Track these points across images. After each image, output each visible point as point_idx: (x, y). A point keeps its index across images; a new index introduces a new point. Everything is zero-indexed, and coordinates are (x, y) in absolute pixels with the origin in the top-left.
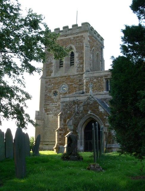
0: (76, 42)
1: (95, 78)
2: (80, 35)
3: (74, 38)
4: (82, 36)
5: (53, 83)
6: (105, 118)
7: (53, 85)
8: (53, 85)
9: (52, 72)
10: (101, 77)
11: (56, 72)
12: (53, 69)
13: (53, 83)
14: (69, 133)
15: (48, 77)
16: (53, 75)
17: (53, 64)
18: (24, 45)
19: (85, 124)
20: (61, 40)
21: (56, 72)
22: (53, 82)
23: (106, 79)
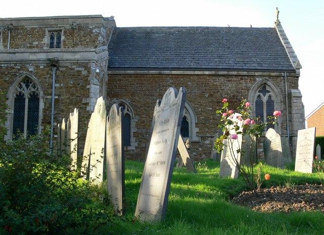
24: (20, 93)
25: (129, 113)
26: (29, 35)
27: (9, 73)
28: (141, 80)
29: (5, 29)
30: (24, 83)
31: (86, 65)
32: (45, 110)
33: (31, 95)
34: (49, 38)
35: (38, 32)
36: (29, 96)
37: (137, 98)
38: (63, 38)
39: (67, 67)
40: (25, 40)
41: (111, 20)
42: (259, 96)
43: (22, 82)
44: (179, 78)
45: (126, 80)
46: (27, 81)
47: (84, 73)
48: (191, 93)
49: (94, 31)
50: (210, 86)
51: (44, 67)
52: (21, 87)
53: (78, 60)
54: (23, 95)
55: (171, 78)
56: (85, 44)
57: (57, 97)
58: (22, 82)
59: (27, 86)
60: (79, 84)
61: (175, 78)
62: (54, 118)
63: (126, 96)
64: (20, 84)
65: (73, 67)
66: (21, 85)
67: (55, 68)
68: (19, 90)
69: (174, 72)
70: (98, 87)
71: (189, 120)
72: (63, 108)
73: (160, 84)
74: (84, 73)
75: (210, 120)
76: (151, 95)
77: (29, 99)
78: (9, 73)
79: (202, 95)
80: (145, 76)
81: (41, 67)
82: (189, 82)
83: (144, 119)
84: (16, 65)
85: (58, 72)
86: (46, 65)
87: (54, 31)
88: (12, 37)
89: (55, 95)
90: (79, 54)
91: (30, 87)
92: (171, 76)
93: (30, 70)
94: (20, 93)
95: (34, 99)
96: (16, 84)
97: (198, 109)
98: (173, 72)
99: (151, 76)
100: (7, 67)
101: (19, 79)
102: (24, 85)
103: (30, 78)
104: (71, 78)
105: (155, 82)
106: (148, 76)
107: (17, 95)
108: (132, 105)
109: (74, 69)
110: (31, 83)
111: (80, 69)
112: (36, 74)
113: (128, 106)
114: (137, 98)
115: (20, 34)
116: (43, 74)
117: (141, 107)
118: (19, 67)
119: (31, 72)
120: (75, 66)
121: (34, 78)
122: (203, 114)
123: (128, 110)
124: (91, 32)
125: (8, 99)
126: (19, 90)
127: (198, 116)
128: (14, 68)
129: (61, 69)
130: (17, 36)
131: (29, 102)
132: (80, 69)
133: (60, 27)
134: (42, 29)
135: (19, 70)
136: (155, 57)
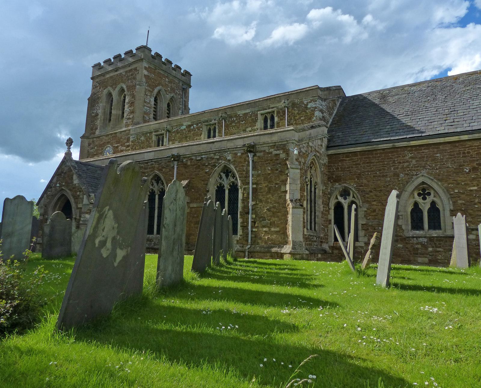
0: (128, 80)
1: (143, 134)
2: (133, 67)
3: (126, 72)
4: (136, 69)
5: (96, 146)
6: (79, 196)
7: (96, 148)
8: (96, 148)
9: (97, 129)
10: (151, 133)
11: (104, 126)
12: (98, 123)
13: (96, 146)
14: (212, 257)
15: (92, 136)
16: (97, 132)
17: (99, 117)
18: (213, 37)
19: (60, 203)
20: (111, 77)
21: (104, 126)
22: (97, 143)
23: (157, 135)
24: (221, 184)
25: (355, 200)
26: (242, 121)
27: (209, 164)
28: (370, 158)
29: (220, 119)
30: (224, 173)
31: (283, 147)
32: (243, 200)
33: (230, 186)
34: (263, 121)
35: (251, 117)
36: (229, 186)
37: (365, 181)
38: (276, 119)
39: (264, 151)
40: (238, 128)
41: (337, 91)
42: (416, 204)
43: (221, 172)
44: (421, 150)
45: (349, 160)
46: (227, 172)
47: (283, 156)
48: (440, 168)
49: (309, 106)
50: (472, 155)
51: (242, 154)
52: (221, 178)
53: (275, 142)
54: (224, 186)
55: (409, 151)
56: (300, 122)
57: (255, 186)
58: (221, 172)
59: (227, 176)
60: (277, 170)
61: (415, 150)
62: (252, 210)
63: (351, 179)
64: (220, 174)
65: (271, 150)
66: (221, 176)
67: (252, 154)
68: (151, 187)
69: (413, 143)
70: (299, 171)
71: (439, 206)
72: (261, 197)
73: (395, 161)
74: (283, 156)
75: (475, 204)
76: (383, 176)
77: (229, 190)
78: (209, 164)
79: (459, 170)
80: (374, 152)
81: (239, 154)
82: (437, 154)
83: (375, 207)
84: (215, 154)
85: (255, 158)
86: (242, 151)
87: (267, 113)
88: (227, 126)
89: (253, 184)
90: (276, 135)
91: (229, 177)
92: (409, 149)
93: (228, 158)
94: (221, 184)
95: (234, 189)
96: (216, 175)
97: (453, 190)
98: (411, 142)
99: (382, 151)
100: (207, 158)
101: (218, 169)
102: (224, 176)
103: (229, 168)
104: (269, 163)
105: (388, 159)
106: (378, 152)
107: (218, 187)
108: (359, 190)
109: (271, 153)
110: (230, 172)
111: (278, 152)
112: (234, 163)
113: (353, 192)
114: (365, 181)
115: (234, 121)
116: (240, 162)
117: (371, 192)
118: (218, 157)
119: (229, 160)
120: (273, 150)
121: (232, 167)
122: (463, 196)
123: (354, 197)
124: (306, 108)
125: (208, 191)
126: (151, 187)
127: (454, 200)
128: (213, 159)
129: (258, 154)
130: (231, 124)
131: (229, 193)
132: (278, 152)
133: (273, 108)
134: (254, 113)
135: (218, 159)
136: (389, 127)
